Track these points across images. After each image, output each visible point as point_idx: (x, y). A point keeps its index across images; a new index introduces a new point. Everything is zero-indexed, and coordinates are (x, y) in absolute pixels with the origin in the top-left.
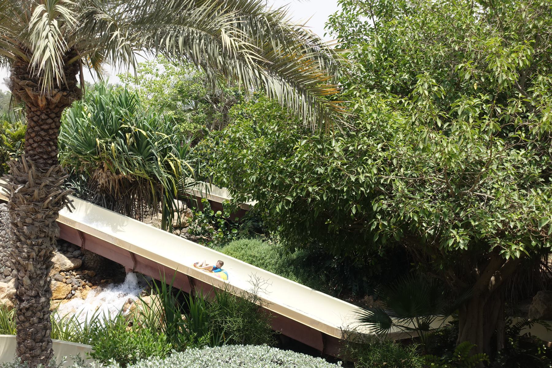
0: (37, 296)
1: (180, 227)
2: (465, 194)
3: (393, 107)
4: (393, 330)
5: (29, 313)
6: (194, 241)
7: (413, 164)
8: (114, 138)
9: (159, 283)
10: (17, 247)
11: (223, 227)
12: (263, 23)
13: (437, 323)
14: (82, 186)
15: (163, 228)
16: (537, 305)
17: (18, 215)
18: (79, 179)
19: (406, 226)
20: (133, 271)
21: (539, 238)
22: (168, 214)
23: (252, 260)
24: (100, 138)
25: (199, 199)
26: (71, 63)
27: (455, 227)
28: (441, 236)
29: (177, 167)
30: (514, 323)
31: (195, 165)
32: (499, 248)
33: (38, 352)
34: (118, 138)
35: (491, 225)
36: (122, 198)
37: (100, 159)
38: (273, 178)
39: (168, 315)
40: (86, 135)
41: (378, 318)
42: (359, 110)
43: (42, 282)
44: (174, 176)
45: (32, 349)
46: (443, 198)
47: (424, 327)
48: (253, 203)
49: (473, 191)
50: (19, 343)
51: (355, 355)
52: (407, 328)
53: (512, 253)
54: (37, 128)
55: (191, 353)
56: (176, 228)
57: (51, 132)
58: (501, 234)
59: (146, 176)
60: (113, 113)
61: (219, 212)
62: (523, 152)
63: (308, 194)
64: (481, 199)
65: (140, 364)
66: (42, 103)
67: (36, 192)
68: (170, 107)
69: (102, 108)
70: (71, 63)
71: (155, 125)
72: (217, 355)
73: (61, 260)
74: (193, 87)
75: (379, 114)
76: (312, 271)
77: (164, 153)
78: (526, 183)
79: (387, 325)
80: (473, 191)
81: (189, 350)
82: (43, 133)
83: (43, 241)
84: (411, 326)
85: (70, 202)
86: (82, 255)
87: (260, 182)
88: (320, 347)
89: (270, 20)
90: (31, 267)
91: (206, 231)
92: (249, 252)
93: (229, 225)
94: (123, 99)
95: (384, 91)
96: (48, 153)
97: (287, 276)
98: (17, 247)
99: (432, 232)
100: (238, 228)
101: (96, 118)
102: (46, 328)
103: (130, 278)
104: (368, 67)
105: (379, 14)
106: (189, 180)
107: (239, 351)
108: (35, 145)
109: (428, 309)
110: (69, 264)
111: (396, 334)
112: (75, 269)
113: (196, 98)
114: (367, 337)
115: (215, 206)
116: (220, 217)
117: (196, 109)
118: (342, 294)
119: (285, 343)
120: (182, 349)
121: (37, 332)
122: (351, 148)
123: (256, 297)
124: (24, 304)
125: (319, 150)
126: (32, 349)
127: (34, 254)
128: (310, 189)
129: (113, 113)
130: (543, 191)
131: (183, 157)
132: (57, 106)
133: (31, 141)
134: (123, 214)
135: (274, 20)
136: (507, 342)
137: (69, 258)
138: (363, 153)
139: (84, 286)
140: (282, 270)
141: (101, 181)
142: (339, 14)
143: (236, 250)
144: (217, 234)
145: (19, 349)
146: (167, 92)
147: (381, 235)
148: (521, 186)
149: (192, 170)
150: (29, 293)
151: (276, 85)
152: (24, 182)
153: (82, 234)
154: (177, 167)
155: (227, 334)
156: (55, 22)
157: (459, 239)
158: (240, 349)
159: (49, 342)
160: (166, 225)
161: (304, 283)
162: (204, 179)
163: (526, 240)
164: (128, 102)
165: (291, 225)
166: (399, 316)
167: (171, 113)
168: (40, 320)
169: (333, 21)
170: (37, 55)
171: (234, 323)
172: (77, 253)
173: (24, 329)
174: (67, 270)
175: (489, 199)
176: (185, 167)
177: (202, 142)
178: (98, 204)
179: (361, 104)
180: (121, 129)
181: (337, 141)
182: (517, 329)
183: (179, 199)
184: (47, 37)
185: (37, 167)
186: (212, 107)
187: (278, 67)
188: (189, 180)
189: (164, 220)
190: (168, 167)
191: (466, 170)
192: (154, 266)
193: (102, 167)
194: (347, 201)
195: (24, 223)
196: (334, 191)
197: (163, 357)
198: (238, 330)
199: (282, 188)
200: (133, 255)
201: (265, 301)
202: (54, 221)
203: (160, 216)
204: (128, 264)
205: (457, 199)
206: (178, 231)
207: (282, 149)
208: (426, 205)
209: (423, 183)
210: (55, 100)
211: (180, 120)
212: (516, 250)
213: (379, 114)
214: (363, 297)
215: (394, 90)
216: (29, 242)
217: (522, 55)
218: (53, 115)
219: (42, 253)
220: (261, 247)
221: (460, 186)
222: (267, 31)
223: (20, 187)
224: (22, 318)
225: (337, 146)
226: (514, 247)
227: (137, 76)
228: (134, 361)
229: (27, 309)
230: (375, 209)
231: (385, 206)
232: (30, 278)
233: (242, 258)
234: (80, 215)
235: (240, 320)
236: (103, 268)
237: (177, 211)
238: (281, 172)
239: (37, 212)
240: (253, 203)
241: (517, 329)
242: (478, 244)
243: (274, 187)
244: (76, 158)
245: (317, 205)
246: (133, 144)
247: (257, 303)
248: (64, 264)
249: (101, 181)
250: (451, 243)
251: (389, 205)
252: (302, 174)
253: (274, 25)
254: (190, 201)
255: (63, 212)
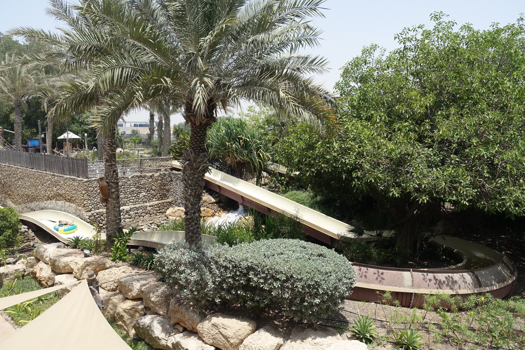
0: (194, 213)
1: (265, 185)
2: (401, 170)
3: (365, 127)
4: (364, 236)
5: (191, 221)
6: (272, 191)
7: (374, 154)
8: (234, 142)
9: (252, 210)
10: (186, 190)
11: (284, 185)
12: (301, 86)
13: (386, 234)
14: (220, 165)
15: (257, 185)
16: (439, 227)
17: (186, 175)
18: (219, 161)
19: (369, 185)
20: (242, 204)
21: (437, 193)
22: (259, 177)
23: (298, 201)
24: (228, 142)
25: (274, 171)
26: (211, 106)
27: (393, 186)
28: (387, 190)
29: (263, 156)
30: (426, 235)
31: (272, 155)
32: (416, 197)
33: (195, 239)
34: (236, 142)
35: (412, 186)
36: (238, 170)
37: (228, 152)
38: (306, 160)
39: (257, 226)
40: (222, 140)
41: (357, 231)
42: (347, 128)
43: (197, 207)
44: (262, 160)
45: (192, 237)
46: (389, 172)
47: (380, 235)
48: (297, 173)
49: (404, 168)
50: (186, 234)
51: (344, 247)
52: (371, 236)
53: (423, 200)
54: (195, 135)
55: (264, 241)
56: (263, 185)
57: (202, 137)
58: (417, 190)
59: (249, 160)
60: (234, 130)
61: (283, 178)
62: (431, 149)
63: (322, 168)
64: (408, 172)
65: (238, 246)
66: (198, 124)
67: (195, 164)
68: (262, 128)
69: (230, 129)
70: (211, 106)
71: (253, 136)
72: (275, 243)
73: (207, 197)
74: (273, 119)
75: (357, 130)
76: (327, 207)
77: (258, 149)
78: (430, 165)
79: (361, 233)
80: (404, 168)
81: (262, 240)
82: (198, 138)
83: (197, 187)
84: (373, 234)
85: (210, 170)
86: (219, 196)
87: (299, 162)
88: (329, 243)
89: (304, 83)
90: (192, 200)
91: (277, 187)
92: (297, 197)
93: (288, 184)
94: (239, 124)
95: (361, 119)
96: (200, 147)
97: (315, 209)
98: (186, 190)
99: (382, 188)
100: (292, 186)
101: (227, 133)
102: (198, 228)
103: (241, 208)
104: (353, 107)
105: (360, 82)
106: (270, 162)
107: (285, 241)
108: (194, 143)
109: (385, 227)
110: (213, 200)
111: (365, 239)
112: (216, 203)
113: (274, 124)
114: (351, 239)
115: (281, 175)
116: (284, 180)
117: (274, 129)
118: (341, 218)
119: (308, 239)
120: (259, 239)
121: (194, 229)
122: (343, 146)
123: (297, 218)
124: (188, 216)
125: (328, 147)
126: (192, 237)
127: (193, 193)
128: (323, 165)
129: (234, 130)
130: (440, 169)
131: (266, 151)
132: (205, 125)
133: (193, 141)
134: (239, 178)
135: (306, 84)
136: (422, 245)
137: (213, 198)
138: (349, 149)
139: (220, 211)
140: (313, 206)
141: (229, 162)
142: (341, 82)
143: (291, 196)
144: (282, 188)
145: (186, 237)
146: (260, 121)
147: (357, 189)
148: (429, 167)
149: (271, 157)
150: (191, 211)
151: (306, 115)
152: (189, 160)
153: (219, 186)
154: (263, 156)
155: (283, 234)
156: (203, 85)
157: (395, 192)
158: (286, 240)
159: (199, 234)
160: (258, 183)
161: (328, 214)
162: (277, 162)
163: (430, 194)
164: (241, 125)
165: (315, 184)
166: (369, 230)
167: (262, 130)
168: (196, 224)
169: (337, 84)
170: (195, 101)
171: (286, 229)
172: (217, 195)
173: (188, 228)
174: (212, 203)
175: (412, 172)
176: (267, 156)
177: (276, 145)
178: (227, 173)
179: (348, 125)
180: (238, 138)
181: (337, 143)
182: (427, 238)
183: (264, 171)
184: (199, 93)
185: (195, 153)
186: (281, 128)
187: (307, 106)
188: (270, 162)
189: (257, 181)
190: (259, 156)
191: (401, 157)
192: (251, 202)
193: (229, 156)
194: (341, 172)
195: (189, 179)
196: (335, 167)
197: (250, 243)
198: (288, 233)
199: (311, 166)
200: (242, 197)
201: (301, 219)
202: (203, 179)
203: (256, 179)
204: (240, 201)
205: (395, 172)
206: (264, 187)
207: (311, 147)
208: (380, 175)
209: (379, 164)
210: (204, 122)
211: (266, 134)
212: (425, 199)
213: (357, 130)
214: (351, 220)
215: (366, 119)
216: (191, 188)
217: (430, 100)
218: (203, 129)
219: (197, 193)
220: (303, 195)
221: (398, 166)
222: (303, 89)
223: (187, 162)
224: (187, 223)
225: (336, 145)
226: (424, 198)
227: (244, 111)
228: (236, 244)
229: (190, 219)
230: (354, 176)
231: (359, 175)
232: (191, 204)
233: (293, 200)
234: (215, 176)
235: (289, 228)
236: (228, 202)
237: (264, 177)
238: (310, 157)
239: (195, 174)
240: (297, 173)
241: (427, 238)
242: (406, 195)
243: (306, 164)
244: (217, 151)
245: (327, 174)
246: (243, 145)
247: (298, 220)
248: (211, 200)
249: (229, 162)
250: (391, 194)
251: (361, 175)
252: (320, 159)
253: (307, 86)
254: (269, 172)
255: (207, 175)
